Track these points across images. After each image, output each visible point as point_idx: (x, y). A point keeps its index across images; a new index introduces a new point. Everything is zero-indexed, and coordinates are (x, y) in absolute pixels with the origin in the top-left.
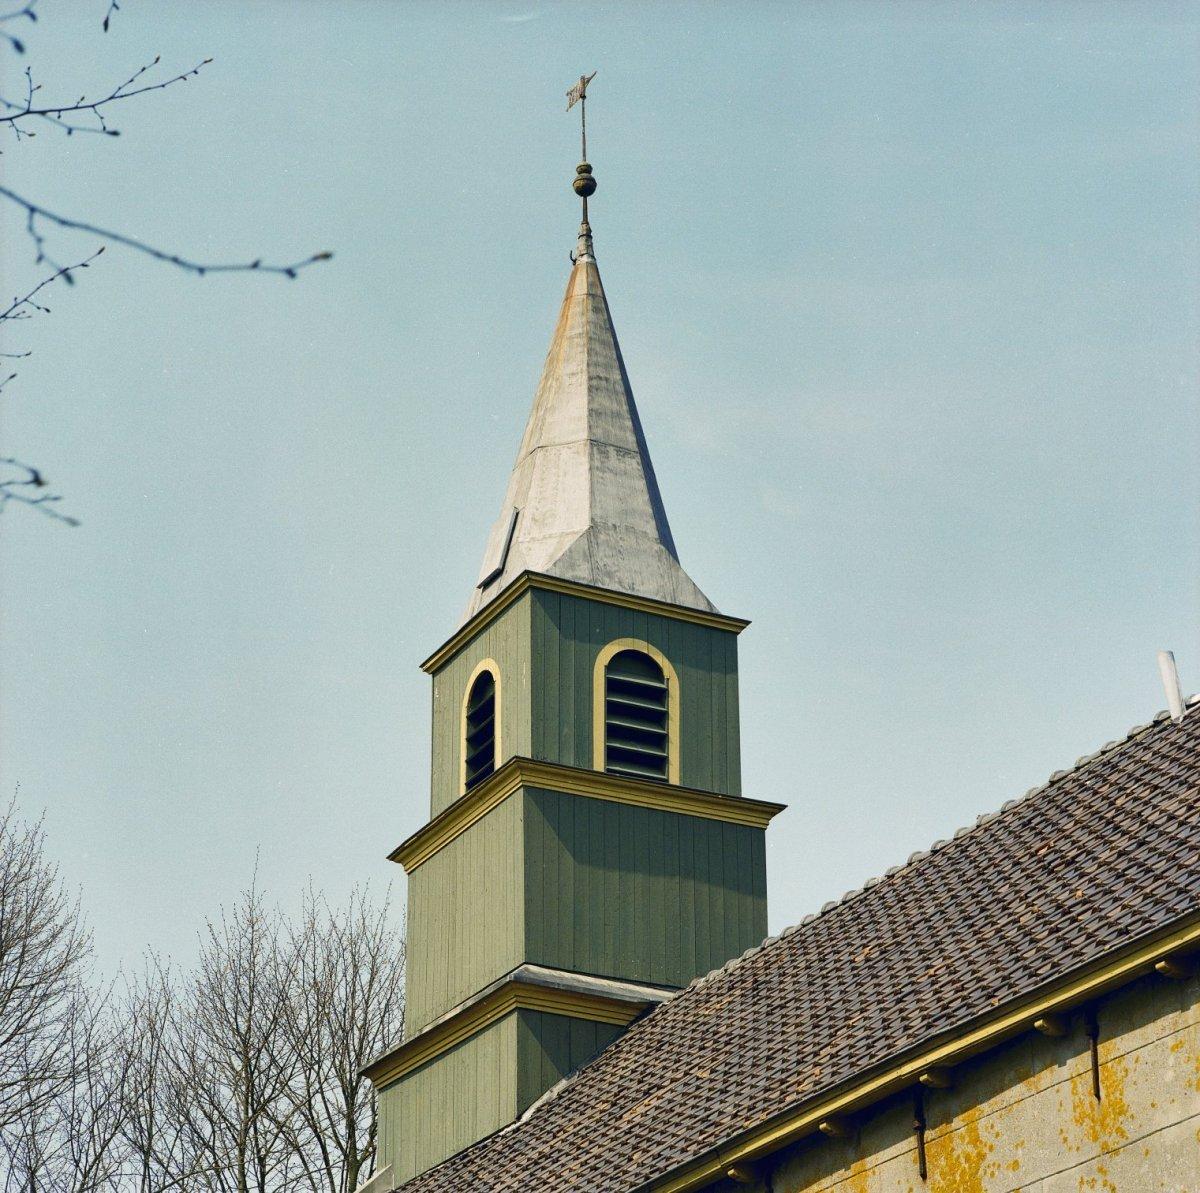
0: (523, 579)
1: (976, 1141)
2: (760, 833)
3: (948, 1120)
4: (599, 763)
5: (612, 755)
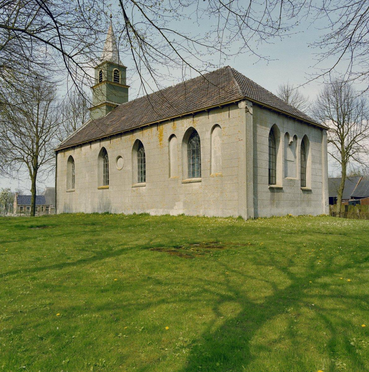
0: (304, 172)
1: (163, 128)
2: (128, 89)
3: (160, 126)
4: (113, 81)
5: (114, 80)
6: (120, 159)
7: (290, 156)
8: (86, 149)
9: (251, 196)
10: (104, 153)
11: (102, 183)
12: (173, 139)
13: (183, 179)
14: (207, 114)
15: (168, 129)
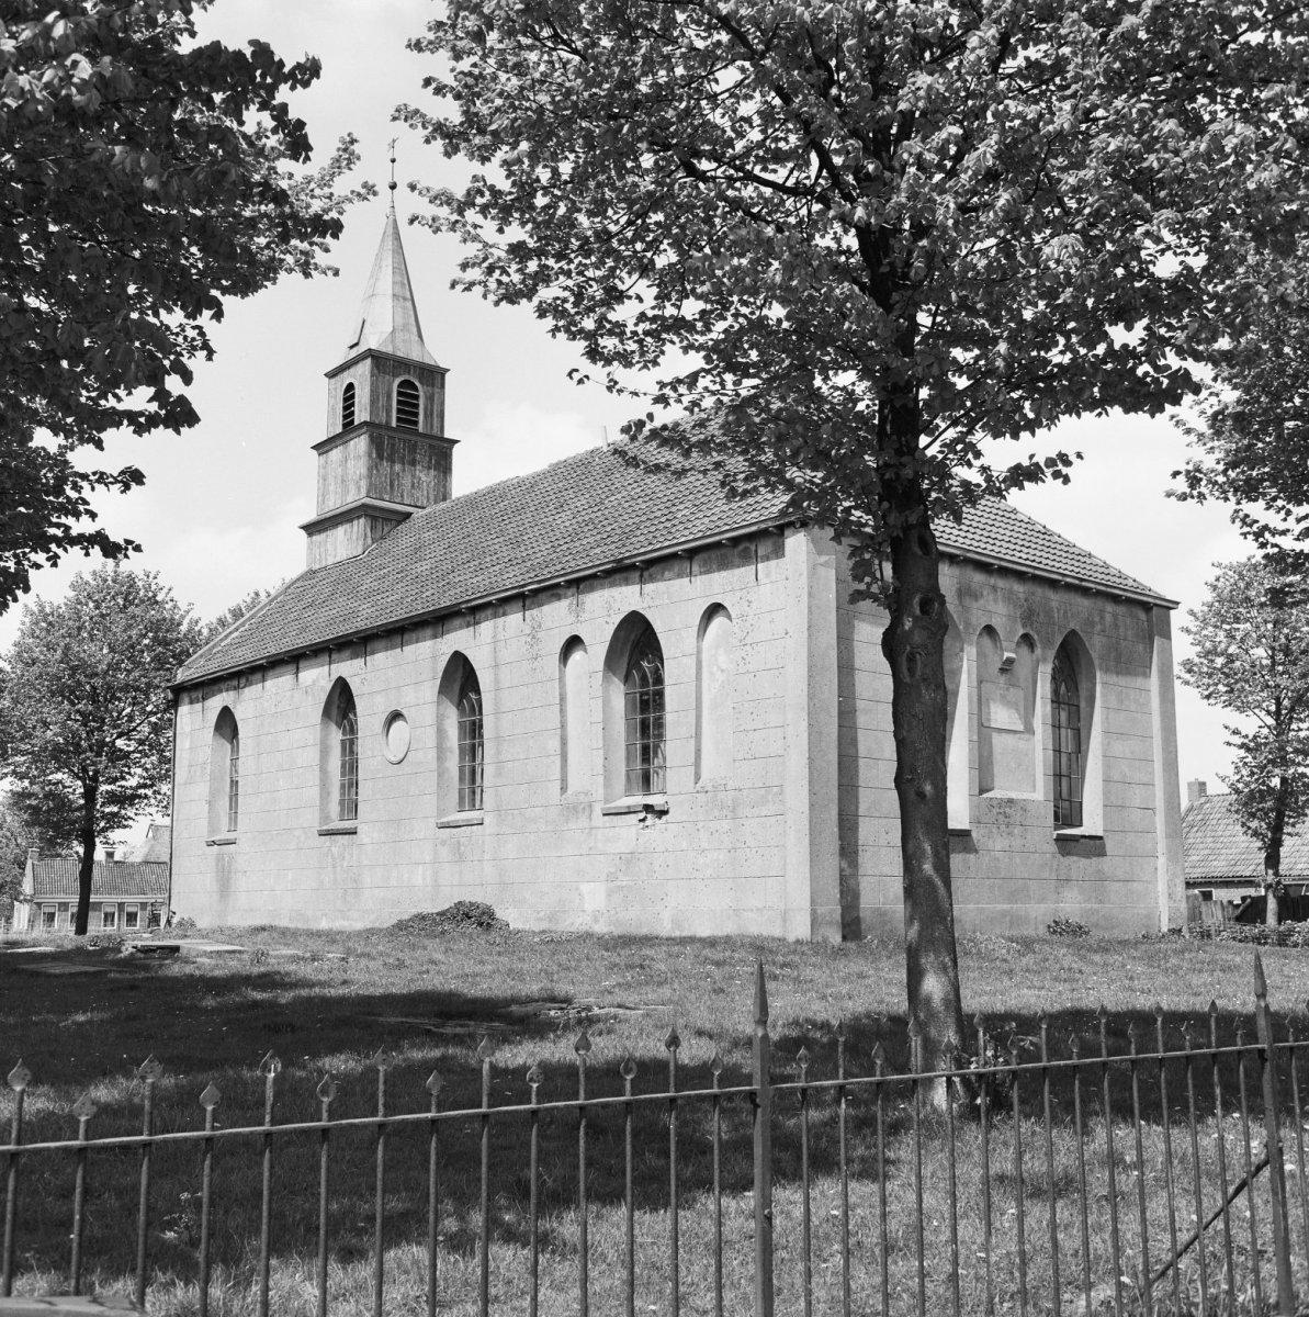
6: (398, 725)
7: (1001, 716)
8: (278, 685)
9: (832, 863)
10: (341, 703)
11: (334, 808)
12: (577, 656)
13: (607, 801)
14: (292, 668)
15: (557, 617)
